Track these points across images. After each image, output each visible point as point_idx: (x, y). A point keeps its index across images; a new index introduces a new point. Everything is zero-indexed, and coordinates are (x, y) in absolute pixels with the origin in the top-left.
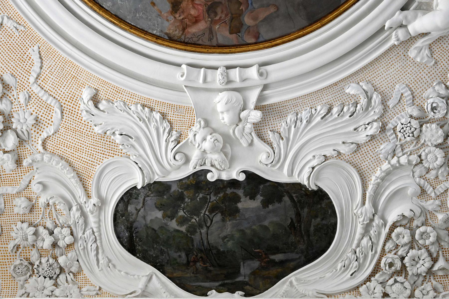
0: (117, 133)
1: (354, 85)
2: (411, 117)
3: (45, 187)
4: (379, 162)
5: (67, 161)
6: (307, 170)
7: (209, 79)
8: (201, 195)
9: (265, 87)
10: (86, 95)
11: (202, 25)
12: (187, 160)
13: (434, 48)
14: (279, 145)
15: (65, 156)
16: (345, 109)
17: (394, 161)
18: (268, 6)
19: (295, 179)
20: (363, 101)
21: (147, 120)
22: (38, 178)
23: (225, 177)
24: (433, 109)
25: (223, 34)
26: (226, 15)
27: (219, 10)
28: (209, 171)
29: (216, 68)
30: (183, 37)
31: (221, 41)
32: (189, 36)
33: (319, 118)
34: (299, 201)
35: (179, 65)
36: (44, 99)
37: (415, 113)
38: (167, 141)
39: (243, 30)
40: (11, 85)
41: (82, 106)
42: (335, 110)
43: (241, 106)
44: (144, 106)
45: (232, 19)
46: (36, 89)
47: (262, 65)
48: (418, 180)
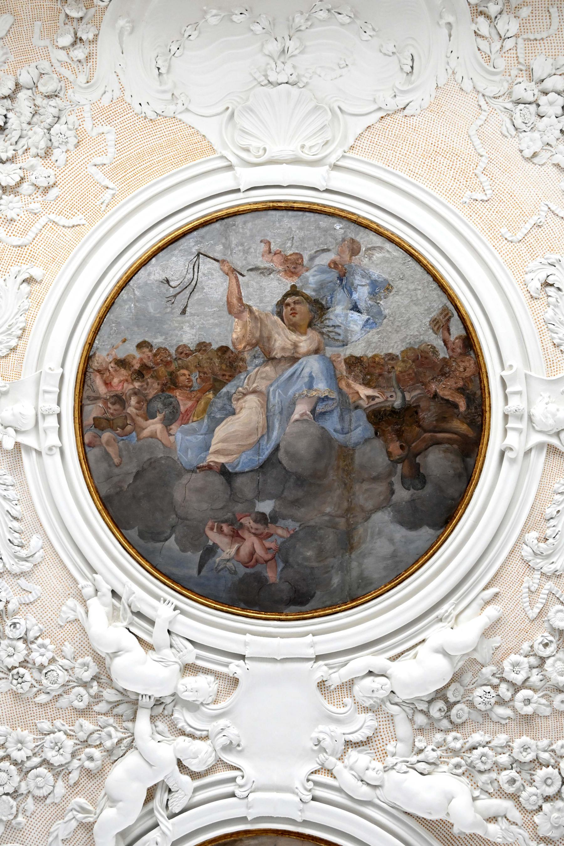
1: (40, 543)
2: (8, 602)
7: (47, 396)
9: (39, 453)
10: (37, 272)
13: (76, 625)
16: (16, 535)
18: (121, 456)
20: (23, 553)
21: (9, 332)
24: (14, 624)
25: (94, 411)
26: (112, 414)
27: (117, 407)
29: (59, 404)
30: (91, 370)
31: (87, 409)
32: (92, 376)
33: (7, 507)
35: (63, 366)
36: (33, 229)
37: (10, 607)
39: (97, 431)
40: (48, 195)
41: (24, 267)
42: (16, 524)
43: (19, 428)
44: (24, 329)
45: (107, 420)
46: (43, 220)
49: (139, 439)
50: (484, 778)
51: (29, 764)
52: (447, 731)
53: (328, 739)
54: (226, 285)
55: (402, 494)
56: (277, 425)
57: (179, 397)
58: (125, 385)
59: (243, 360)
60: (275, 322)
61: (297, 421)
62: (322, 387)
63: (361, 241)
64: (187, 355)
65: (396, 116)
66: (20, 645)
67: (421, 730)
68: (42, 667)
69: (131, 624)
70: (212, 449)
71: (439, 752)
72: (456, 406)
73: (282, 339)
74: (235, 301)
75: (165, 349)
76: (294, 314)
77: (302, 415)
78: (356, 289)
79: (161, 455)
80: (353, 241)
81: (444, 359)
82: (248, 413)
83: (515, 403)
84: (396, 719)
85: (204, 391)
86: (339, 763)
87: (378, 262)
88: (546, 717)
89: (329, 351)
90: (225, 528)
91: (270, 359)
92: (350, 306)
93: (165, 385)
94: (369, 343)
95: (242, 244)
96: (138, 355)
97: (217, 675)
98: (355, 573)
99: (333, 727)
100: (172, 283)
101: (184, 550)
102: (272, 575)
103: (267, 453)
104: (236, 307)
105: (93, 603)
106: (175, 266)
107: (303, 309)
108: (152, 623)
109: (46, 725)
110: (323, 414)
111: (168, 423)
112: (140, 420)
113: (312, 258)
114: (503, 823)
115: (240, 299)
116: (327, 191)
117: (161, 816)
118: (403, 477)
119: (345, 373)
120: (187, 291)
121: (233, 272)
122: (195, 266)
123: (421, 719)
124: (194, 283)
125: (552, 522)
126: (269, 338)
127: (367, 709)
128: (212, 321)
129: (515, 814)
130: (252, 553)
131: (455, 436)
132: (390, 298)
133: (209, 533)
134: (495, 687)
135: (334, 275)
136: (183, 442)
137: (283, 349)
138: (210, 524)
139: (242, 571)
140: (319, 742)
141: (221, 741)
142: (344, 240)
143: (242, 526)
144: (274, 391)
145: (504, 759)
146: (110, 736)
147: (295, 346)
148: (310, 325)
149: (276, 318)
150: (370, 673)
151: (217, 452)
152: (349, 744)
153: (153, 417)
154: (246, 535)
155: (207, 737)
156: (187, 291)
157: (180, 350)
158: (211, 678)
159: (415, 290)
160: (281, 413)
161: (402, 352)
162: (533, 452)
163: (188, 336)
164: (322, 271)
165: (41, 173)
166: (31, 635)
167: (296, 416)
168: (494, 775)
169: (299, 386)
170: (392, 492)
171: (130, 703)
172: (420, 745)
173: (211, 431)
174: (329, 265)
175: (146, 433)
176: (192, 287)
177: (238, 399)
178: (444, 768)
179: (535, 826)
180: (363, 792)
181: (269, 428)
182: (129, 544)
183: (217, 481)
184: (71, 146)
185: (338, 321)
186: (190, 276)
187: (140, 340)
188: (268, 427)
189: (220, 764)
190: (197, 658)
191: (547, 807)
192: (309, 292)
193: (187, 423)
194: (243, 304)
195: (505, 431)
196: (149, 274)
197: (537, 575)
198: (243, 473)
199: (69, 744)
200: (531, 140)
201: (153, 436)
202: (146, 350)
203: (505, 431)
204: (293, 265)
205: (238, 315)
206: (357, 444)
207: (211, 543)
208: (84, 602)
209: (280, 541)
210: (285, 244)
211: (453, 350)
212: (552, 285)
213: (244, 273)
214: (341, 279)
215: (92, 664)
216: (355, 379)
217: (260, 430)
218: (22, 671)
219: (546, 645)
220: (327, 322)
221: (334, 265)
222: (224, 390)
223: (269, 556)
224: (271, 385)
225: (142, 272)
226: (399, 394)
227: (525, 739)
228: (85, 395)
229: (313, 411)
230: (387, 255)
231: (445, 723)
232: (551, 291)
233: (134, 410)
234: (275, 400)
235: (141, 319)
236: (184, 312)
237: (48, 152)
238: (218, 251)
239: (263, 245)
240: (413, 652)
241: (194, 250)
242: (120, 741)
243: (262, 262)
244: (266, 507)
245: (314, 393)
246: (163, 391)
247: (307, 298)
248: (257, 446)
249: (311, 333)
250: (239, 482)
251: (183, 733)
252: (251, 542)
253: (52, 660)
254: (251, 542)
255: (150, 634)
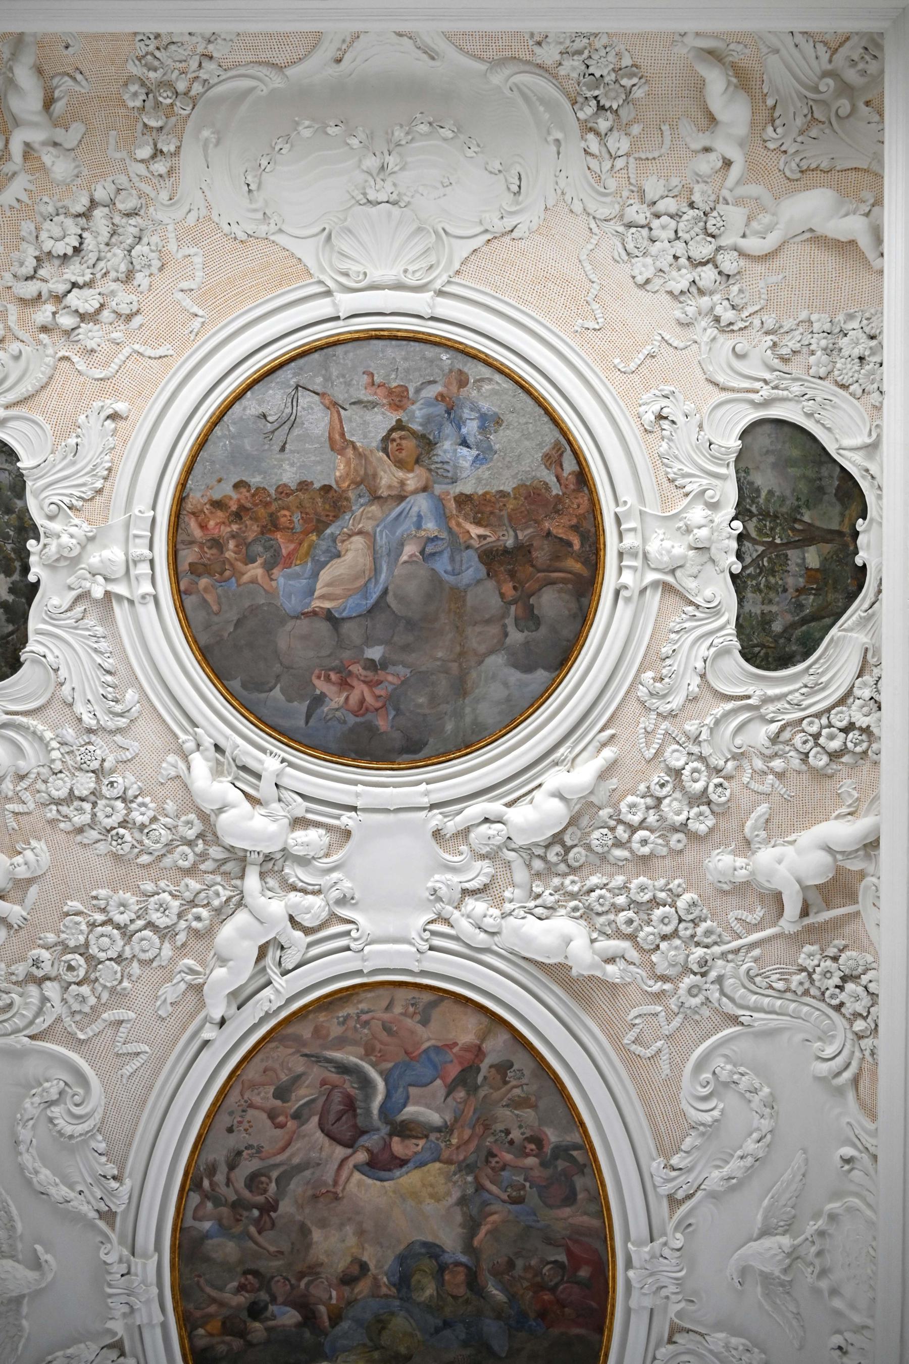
0: (79, 440)
3: (17, 358)
4: (54, 728)
5: (47, 384)
6: (42, 650)
8: (12, 533)
11: (197, 533)
12: (51, 518)
14: (69, 618)
15: (53, 382)
17: (54, 744)
18: (219, 604)
19: (32, 637)
22: (27, 350)
23: (33, 559)
25: (188, 556)
26: (209, 559)
27: (214, 551)
28: (38, 540)
32: (186, 519)
33: (99, 661)
34: (8, 642)
36: (116, 360)
38: (71, 495)
39: (193, 577)
41: (108, 402)
42: (109, 678)
43: (108, 576)
45: (204, 565)
46: (126, 351)
47: (156, 599)
48: (35, 771)
49: (239, 585)
50: (602, 919)
51: (132, 927)
52: (565, 875)
53: (444, 888)
54: (327, 419)
55: (516, 637)
56: (385, 568)
57: (280, 540)
58: (222, 527)
59: (347, 499)
60: (380, 459)
61: (405, 562)
62: (431, 527)
63: (470, 373)
64: (288, 495)
65: (503, 239)
66: (119, 805)
67: (538, 875)
68: (143, 826)
69: (236, 778)
70: (317, 594)
71: (557, 897)
72: (569, 544)
73: (388, 476)
74: (337, 437)
75: (264, 489)
76: (400, 450)
77: (411, 556)
78: (464, 423)
79: (262, 601)
80: (461, 372)
81: (558, 495)
82: (355, 553)
83: (630, 541)
84: (514, 865)
85: (306, 533)
86: (457, 914)
87: (487, 395)
88: (663, 857)
89: (438, 489)
90: (333, 676)
91: (376, 498)
92: (459, 441)
93: (263, 527)
94: (479, 480)
95: (343, 376)
96: (235, 496)
97: (328, 828)
98: (468, 719)
99: (449, 876)
100: (269, 418)
101: (290, 700)
102: (382, 724)
103: (375, 597)
104: (338, 443)
105: (197, 759)
106: (273, 399)
107: (410, 444)
108: (258, 777)
109: (149, 887)
110: (433, 554)
111: (269, 567)
112: (239, 565)
113: (418, 391)
114: (621, 964)
115: (343, 435)
116: (433, 319)
117: (273, 973)
118: (516, 619)
119: (454, 512)
120: (286, 427)
121: (334, 406)
122: (294, 400)
123: (538, 864)
124: (293, 418)
125: (668, 662)
126: (375, 476)
127: (483, 857)
128: (313, 458)
129: (633, 954)
130: (362, 701)
131: (569, 576)
132: (501, 433)
133: (316, 682)
134: (612, 829)
135: (441, 408)
136: (286, 586)
137: (390, 487)
138: (317, 672)
139: (352, 720)
140: (435, 891)
141: (334, 894)
142: (451, 371)
143: (350, 674)
144: (381, 531)
145: (621, 900)
146: (218, 894)
147: (402, 483)
148: (417, 461)
149: (381, 454)
150: (486, 820)
151: (323, 597)
152: (465, 892)
153: (253, 561)
154: (355, 683)
155: (318, 892)
156: (286, 427)
157: (280, 490)
158: (322, 831)
159: (527, 423)
160: (388, 555)
161: (514, 489)
162: (648, 591)
163: (289, 475)
164: (428, 404)
165: (123, 299)
166: (130, 793)
167: (404, 558)
168: (611, 917)
169: (407, 526)
170: (506, 635)
171: (237, 861)
172: (537, 890)
173: (315, 575)
174: (436, 398)
175: (245, 578)
176: (290, 422)
177: (343, 541)
178: (562, 911)
179: (653, 965)
180: (481, 939)
181: (376, 571)
182: (231, 696)
183: (324, 627)
184: (154, 269)
185: (447, 457)
186: (288, 410)
187: (238, 480)
188: (375, 569)
189: (334, 918)
190: (308, 811)
191: (664, 945)
192: (415, 427)
193: (290, 567)
194: (346, 440)
195: (620, 570)
196: (245, 409)
197: (653, 716)
198: (350, 618)
199: (175, 904)
200: (644, 266)
201: (254, 581)
202: (243, 490)
203: (620, 570)
204: (398, 399)
205: (341, 452)
206: (469, 585)
207: (318, 692)
208: (185, 757)
209: (390, 688)
210: (389, 375)
211: (566, 486)
212: (666, 418)
213: (347, 406)
214: (448, 412)
215: (196, 822)
216: (466, 518)
217: (367, 573)
218: (122, 831)
219: (662, 786)
220: (436, 459)
221: (441, 397)
222: (328, 531)
223: (379, 704)
224: (378, 526)
225: (237, 407)
226: (512, 533)
227: (642, 879)
228: (179, 539)
229: (422, 552)
230: (497, 387)
231: (563, 867)
232: (665, 424)
233: (233, 555)
234: (382, 541)
235: (236, 457)
236: (283, 449)
237: (129, 276)
238: (318, 383)
239: (365, 376)
240: (529, 797)
241: (293, 382)
242: (229, 899)
243: (365, 395)
244: (375, 653)
245: (423, 533)
246: (262, 533)
247: (414, 433)
248: (364, 590)
249: (419, 470)
250: (346, 627)
251: (294, 888)
252: (360, 690)
253: (154, 819)
254: (360, 690)
255: (256, 788)
